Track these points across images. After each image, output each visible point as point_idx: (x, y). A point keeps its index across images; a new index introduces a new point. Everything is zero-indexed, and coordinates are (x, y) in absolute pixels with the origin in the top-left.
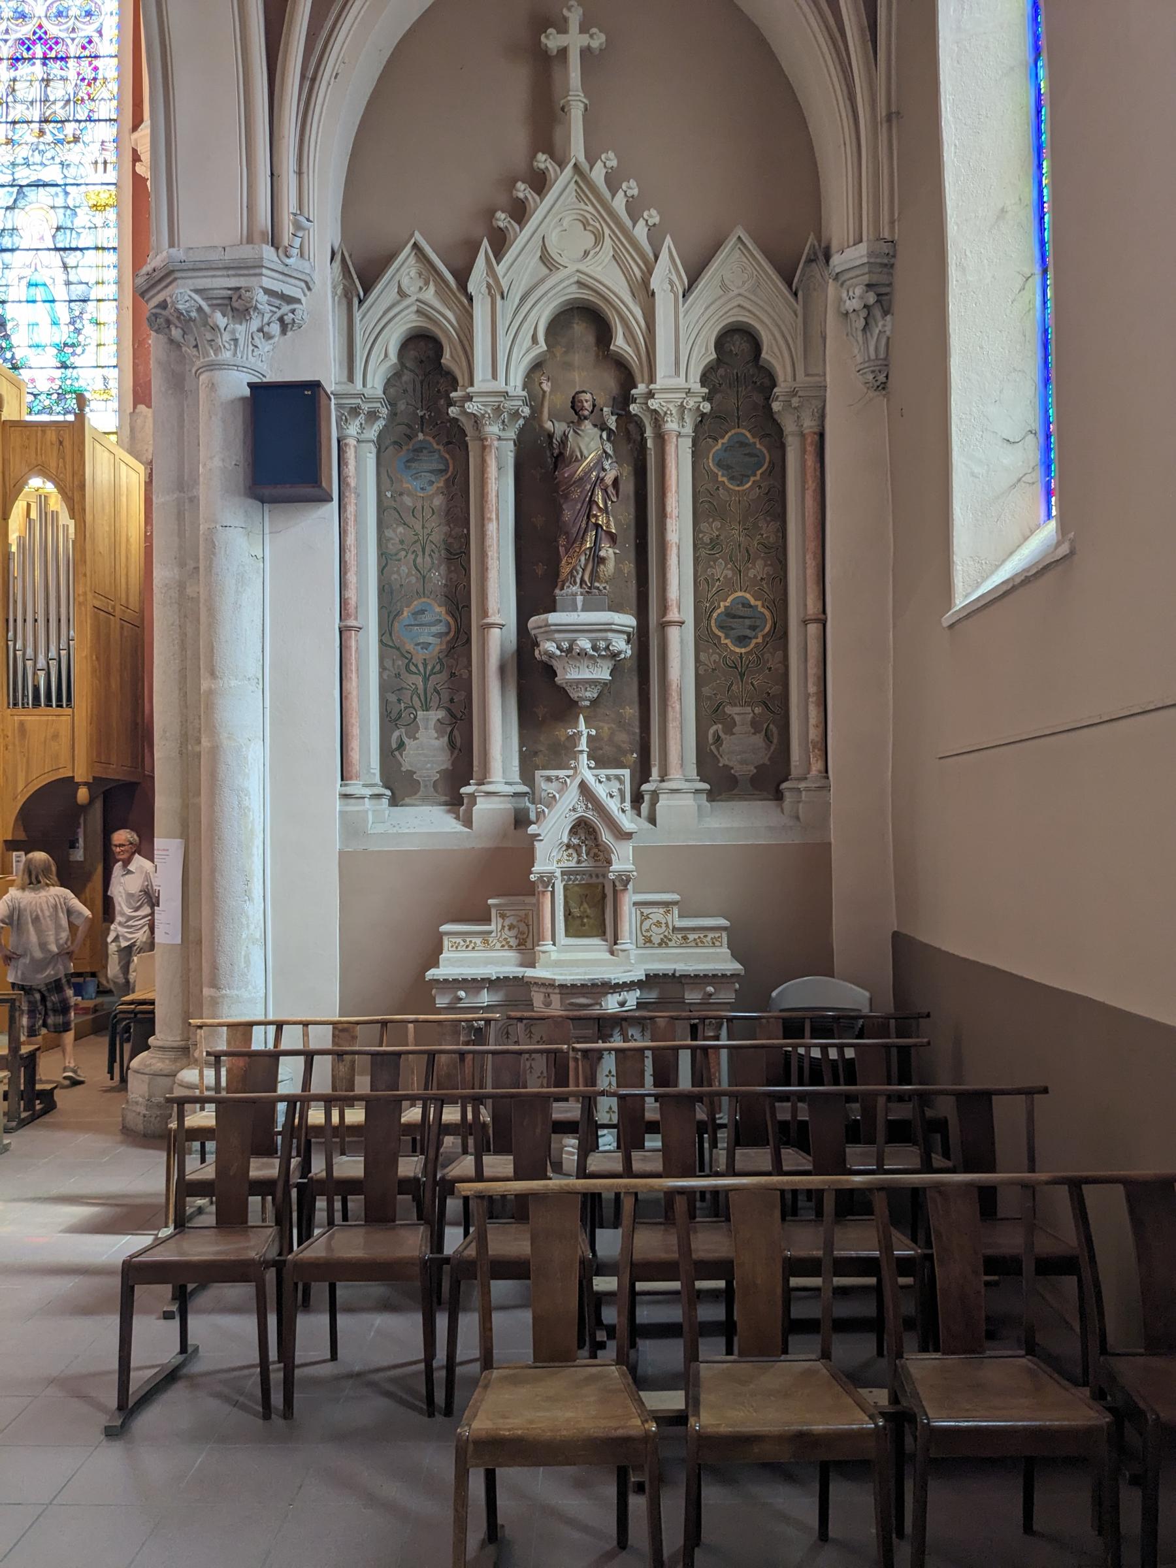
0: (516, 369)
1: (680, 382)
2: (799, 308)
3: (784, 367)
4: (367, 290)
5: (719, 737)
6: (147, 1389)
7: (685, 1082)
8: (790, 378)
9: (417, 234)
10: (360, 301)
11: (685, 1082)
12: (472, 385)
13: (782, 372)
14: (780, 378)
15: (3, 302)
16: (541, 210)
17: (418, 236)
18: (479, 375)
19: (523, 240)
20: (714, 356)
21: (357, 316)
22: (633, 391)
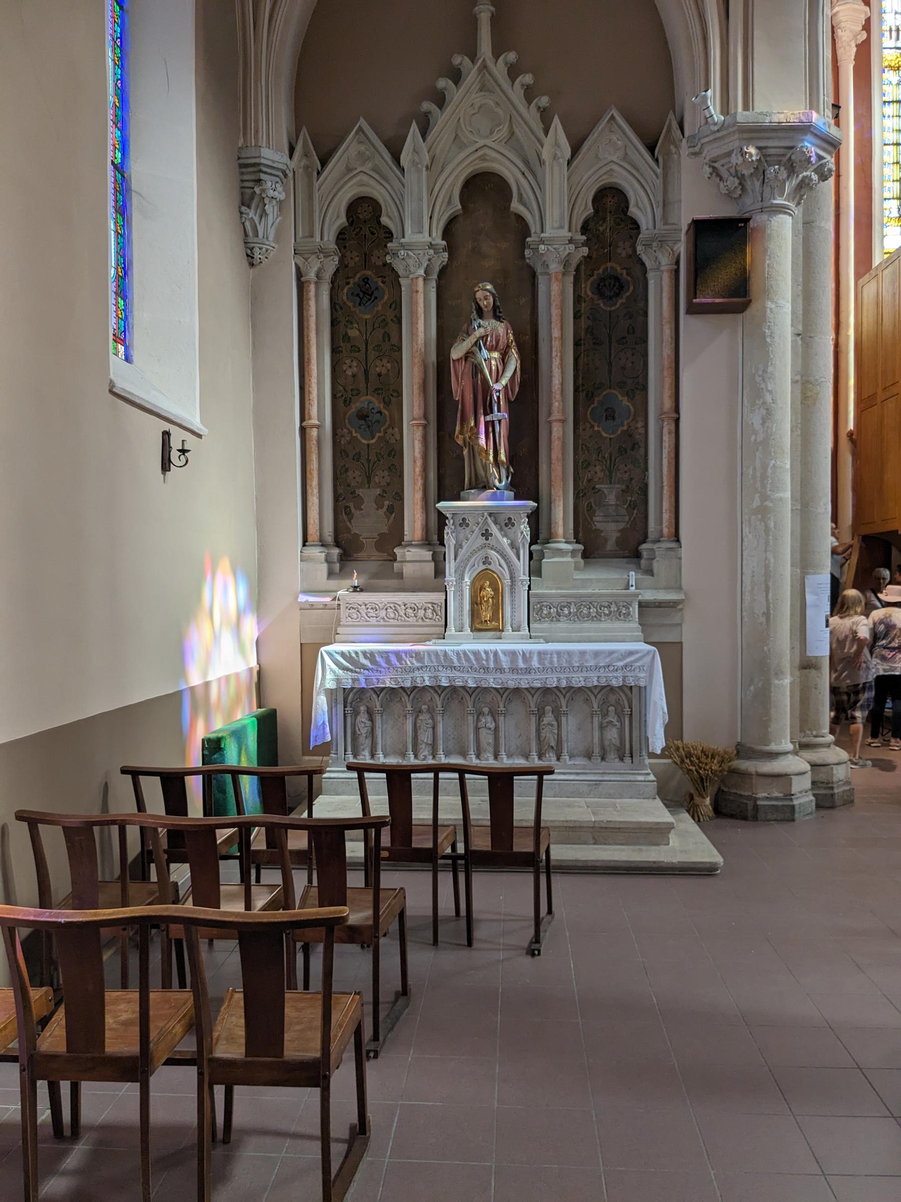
0: (329, 229)
1: (425, 238)
2: (659, 171)
3: (535, 223)
4: (324, 163)
5: (591, 507)
6: (646, 865)
7: (195, 809)
8: (651, 226)
9: (362, 119)
10: (319, 173)
11: (195, 809)
12: (404, 237)
13: (645, 222)
14: (643, 227)
15: (898, 144)
16: (455, 95)
17: (362, 122)
18: (408, 230)
19: (442, 121)
20: (592, 211)
21: (316, 185)
22: (528, 239)
